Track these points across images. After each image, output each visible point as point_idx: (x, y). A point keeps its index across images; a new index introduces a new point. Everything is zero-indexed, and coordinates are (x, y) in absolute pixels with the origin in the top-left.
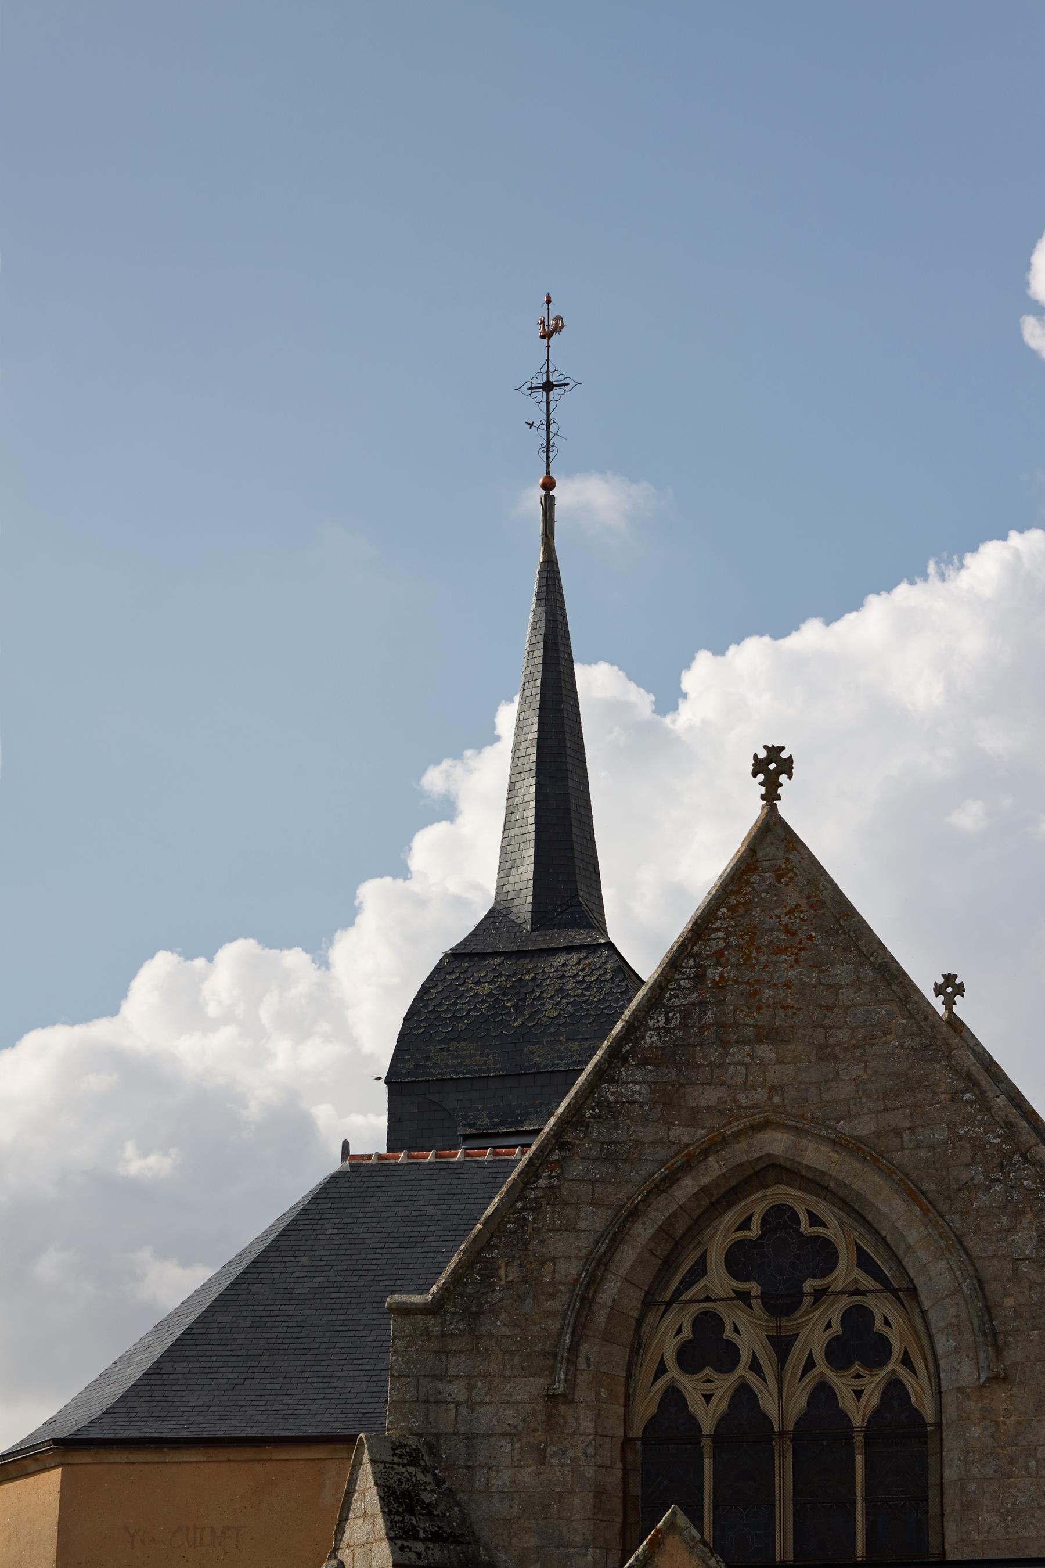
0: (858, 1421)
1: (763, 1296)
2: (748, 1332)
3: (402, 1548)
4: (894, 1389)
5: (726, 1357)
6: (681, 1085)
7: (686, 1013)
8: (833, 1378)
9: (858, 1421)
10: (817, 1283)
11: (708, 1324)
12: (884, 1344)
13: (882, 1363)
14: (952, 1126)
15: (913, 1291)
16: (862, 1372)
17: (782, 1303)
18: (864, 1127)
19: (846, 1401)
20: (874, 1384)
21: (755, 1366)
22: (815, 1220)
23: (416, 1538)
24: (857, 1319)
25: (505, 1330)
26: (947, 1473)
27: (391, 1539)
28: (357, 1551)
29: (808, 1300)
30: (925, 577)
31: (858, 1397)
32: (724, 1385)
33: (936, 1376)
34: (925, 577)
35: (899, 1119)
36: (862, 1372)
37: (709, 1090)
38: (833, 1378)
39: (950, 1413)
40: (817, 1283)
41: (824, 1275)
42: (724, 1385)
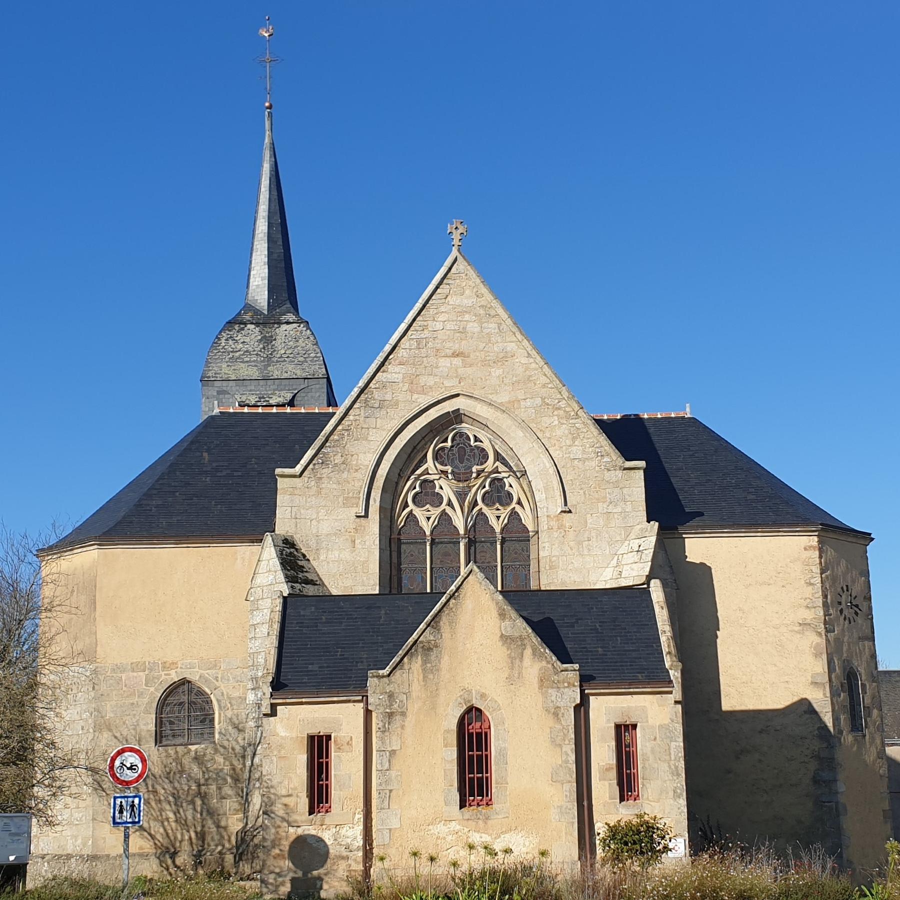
0: (498, 530)
1: (453, 473)
2: (446, 489)
3: (292, 587)
4: (514, 514)
5: (437, 499)
6: (418, 375)
7: (419, 341)
8: (486, 510)
9: (498, 530)
10: (479, 467)
11: (428, 485)
12: (510, 495)
13: (509, 504)
14: (543, 399)
15: (524, 473)
16: (500, 507)
17: (461, 476)
18: (502, 398)
19: (493, 521)
20: (505, 513)
21: (450, 503)
22: (476, 439)
23: (297, 582)
24: (497, 484)
25: (334, 486)
26: (541, 553)
27: (287, 582)
28: (265, 588)
29: (474, 475)
30: (320, 879)
31: (496, 518)
32: (435, 512)
33: (535, 509)
34: (320, 879)
35: (520, 395)
36: (500, 507)
37: (431, 378)
38: (486, 510)
39: (543, 526)
40: (479, 467)
41: (482, 464)
42: (435, 512)
